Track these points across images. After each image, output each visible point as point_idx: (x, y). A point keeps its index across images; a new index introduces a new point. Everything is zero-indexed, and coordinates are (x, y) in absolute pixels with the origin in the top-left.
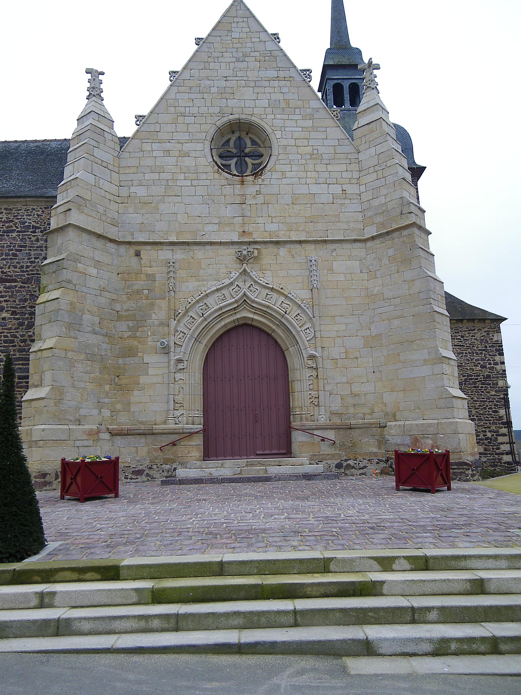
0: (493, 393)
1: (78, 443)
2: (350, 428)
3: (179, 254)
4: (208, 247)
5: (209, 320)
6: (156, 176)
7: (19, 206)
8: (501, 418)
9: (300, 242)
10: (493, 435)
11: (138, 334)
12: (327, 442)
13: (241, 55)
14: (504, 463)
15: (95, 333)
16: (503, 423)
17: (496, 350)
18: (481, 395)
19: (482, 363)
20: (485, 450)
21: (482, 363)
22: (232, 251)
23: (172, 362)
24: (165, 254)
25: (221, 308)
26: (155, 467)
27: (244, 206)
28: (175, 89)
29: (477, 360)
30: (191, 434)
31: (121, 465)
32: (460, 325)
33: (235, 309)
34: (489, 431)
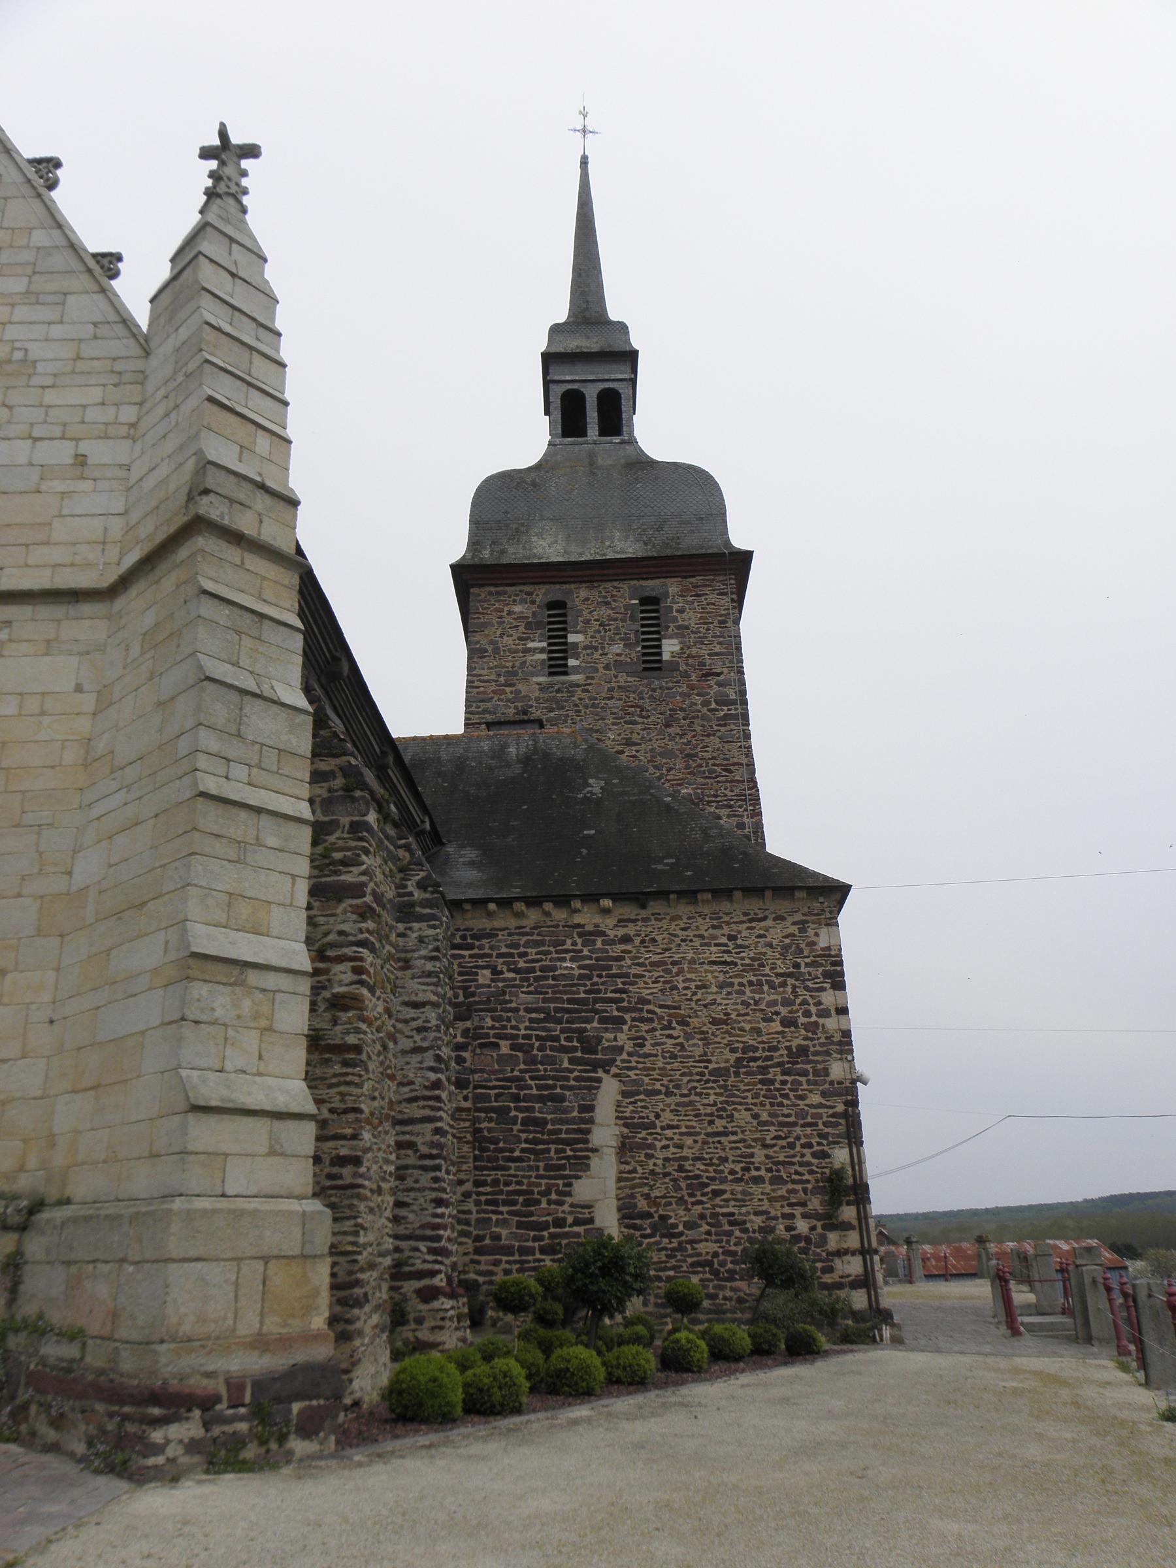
0: (816, 1099)
10: (813, 1228)
17: (826, 975)
19: (784, 1011)
21: (784, 1011)
32: (726, 906)
34: (805, 1216)
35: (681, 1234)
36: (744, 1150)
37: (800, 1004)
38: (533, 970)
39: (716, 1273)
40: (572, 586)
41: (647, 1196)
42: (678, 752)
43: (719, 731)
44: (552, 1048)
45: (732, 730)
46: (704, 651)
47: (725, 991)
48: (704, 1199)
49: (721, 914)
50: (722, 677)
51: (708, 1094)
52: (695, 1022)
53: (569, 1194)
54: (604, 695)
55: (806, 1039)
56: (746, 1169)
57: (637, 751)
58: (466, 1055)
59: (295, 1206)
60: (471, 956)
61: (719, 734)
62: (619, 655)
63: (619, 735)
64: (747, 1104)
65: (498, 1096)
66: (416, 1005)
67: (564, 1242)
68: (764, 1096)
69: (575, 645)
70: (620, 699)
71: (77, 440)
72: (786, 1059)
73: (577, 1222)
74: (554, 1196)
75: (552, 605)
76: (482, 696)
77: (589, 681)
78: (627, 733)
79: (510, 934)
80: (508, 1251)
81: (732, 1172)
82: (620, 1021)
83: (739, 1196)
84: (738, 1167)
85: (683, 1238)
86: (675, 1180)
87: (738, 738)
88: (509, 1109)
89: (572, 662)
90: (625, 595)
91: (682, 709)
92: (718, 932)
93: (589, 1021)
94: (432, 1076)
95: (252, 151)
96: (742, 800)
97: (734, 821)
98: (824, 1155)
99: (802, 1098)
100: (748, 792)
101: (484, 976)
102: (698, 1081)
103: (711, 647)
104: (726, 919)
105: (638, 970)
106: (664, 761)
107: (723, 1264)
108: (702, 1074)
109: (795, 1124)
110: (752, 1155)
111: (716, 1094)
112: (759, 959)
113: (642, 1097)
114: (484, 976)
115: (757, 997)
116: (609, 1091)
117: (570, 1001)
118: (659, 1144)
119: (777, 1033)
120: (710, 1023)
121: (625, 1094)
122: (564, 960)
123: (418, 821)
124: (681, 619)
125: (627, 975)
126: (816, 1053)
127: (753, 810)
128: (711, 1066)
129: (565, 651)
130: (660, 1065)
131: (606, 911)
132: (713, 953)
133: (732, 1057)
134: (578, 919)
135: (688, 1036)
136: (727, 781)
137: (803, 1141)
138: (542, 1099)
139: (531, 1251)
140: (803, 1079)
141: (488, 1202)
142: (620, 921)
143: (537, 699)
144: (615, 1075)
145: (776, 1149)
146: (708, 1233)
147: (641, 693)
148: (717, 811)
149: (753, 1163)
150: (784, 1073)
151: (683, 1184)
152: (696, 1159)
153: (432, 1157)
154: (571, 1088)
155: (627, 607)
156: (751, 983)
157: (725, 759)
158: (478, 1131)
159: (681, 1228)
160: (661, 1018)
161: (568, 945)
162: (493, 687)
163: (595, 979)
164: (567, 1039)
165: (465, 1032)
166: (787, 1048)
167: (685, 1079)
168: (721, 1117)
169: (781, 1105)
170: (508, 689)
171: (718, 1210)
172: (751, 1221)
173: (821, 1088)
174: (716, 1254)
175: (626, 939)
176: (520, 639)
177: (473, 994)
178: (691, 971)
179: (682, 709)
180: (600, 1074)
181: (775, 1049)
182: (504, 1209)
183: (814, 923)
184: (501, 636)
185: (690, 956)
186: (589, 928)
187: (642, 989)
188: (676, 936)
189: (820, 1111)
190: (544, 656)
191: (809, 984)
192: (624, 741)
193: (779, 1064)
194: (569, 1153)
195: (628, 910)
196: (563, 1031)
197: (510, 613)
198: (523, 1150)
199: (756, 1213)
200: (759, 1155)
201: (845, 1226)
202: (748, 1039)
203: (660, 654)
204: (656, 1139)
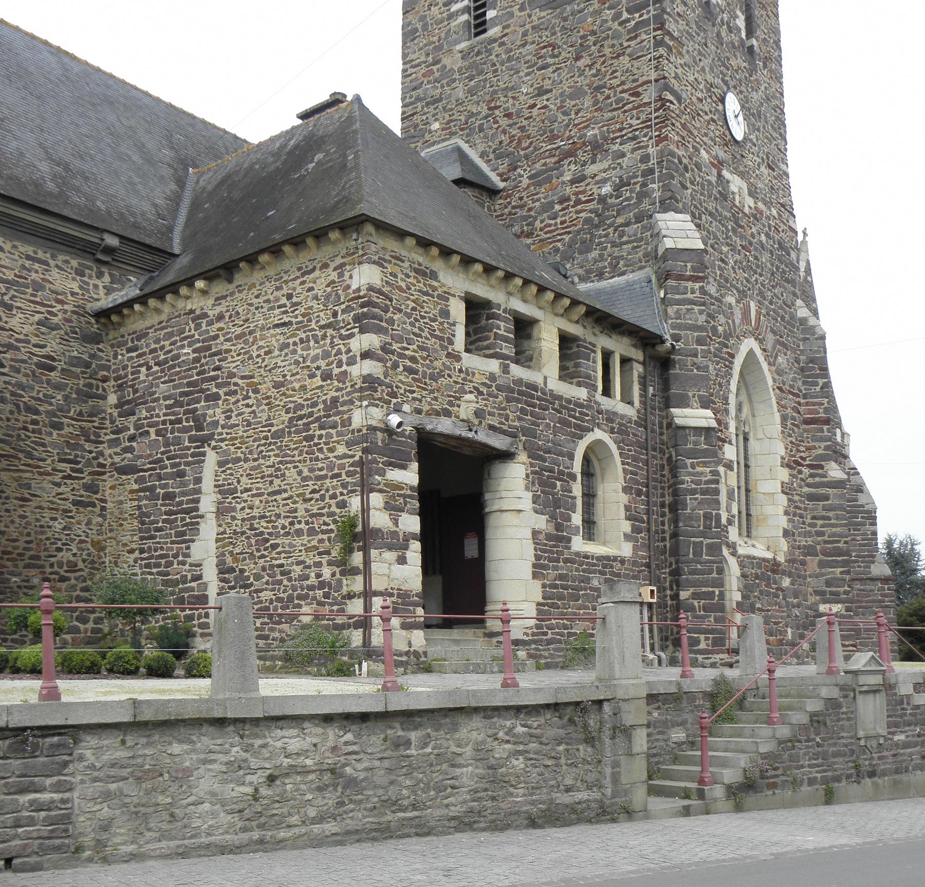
10: (333, 575)
21: (322, 363)
29: (315, 359)
35: (252, 584)
36: (292, 505)
37: (335, 355)
39: (270, 616)
42: (586, 88)
43: (629, 46)
45: (642, 41)
48: (266, 553)
49: (282, 274)
51: (269, 457)
54: (518, 43)
56: (292, 524)
57: (548, 100)
61: (628, 51)
63: (532, 86)
64: (294, 462)
67: (186, 595)
68: (307, 453)
70: (533, 42)
72: (322, 413)
74: (181, 558)
76: (414, 84)
77: (506, 31)
78: (539, 81)
81: (284, 527)
82: (216, 397)
83: (287, 549)
85: (252, 588)
86: (248, 538)
87: (648, 49)
91: (593, 33)
96: (648, 127)
99: (331, 450)
100: (654, 115)
102: (264, 445)
106: (573, 103)
108: (266, 438)
109: (325, 477)
110: (296, 511)
111: (275, 455)
113: (230, 465)
116: (211, 458)
118: (239, 507)
119: (318, 388)
120: (273, 387)
123: (97, 241)
127: (658, 136)
128: (273, 429)
130: (241, 434)
132: (276, 316)
136: (635, 108)
140: (333, 431)
142: (217, 299)
144: (214, 448)
145: (313, 502)
146: (267, 583)
147: (553, 27)
148: (621, 148)
149: (296, 517)
150: (321, 428)
156: (302, 341)
157: (634, 81)
159: (252, 579)
163: (203, 361)
166: (324, 402)
169: (317, 459)
172: (294, 571)
173: (346, 438)
174: (271, 601)
180: (207, 449)
181: (314, 405)
183: (350, 264)
187: (229, 365)
188: (251, 305)
189: (344, 461)
190: (465, 17)
191: (343, 332)
192: (536, 92)
193: (318, 419)
195: (220, 288)
198: (164, 521)
200: (301, 507)
201: (354, 571)
204: (237, 502)
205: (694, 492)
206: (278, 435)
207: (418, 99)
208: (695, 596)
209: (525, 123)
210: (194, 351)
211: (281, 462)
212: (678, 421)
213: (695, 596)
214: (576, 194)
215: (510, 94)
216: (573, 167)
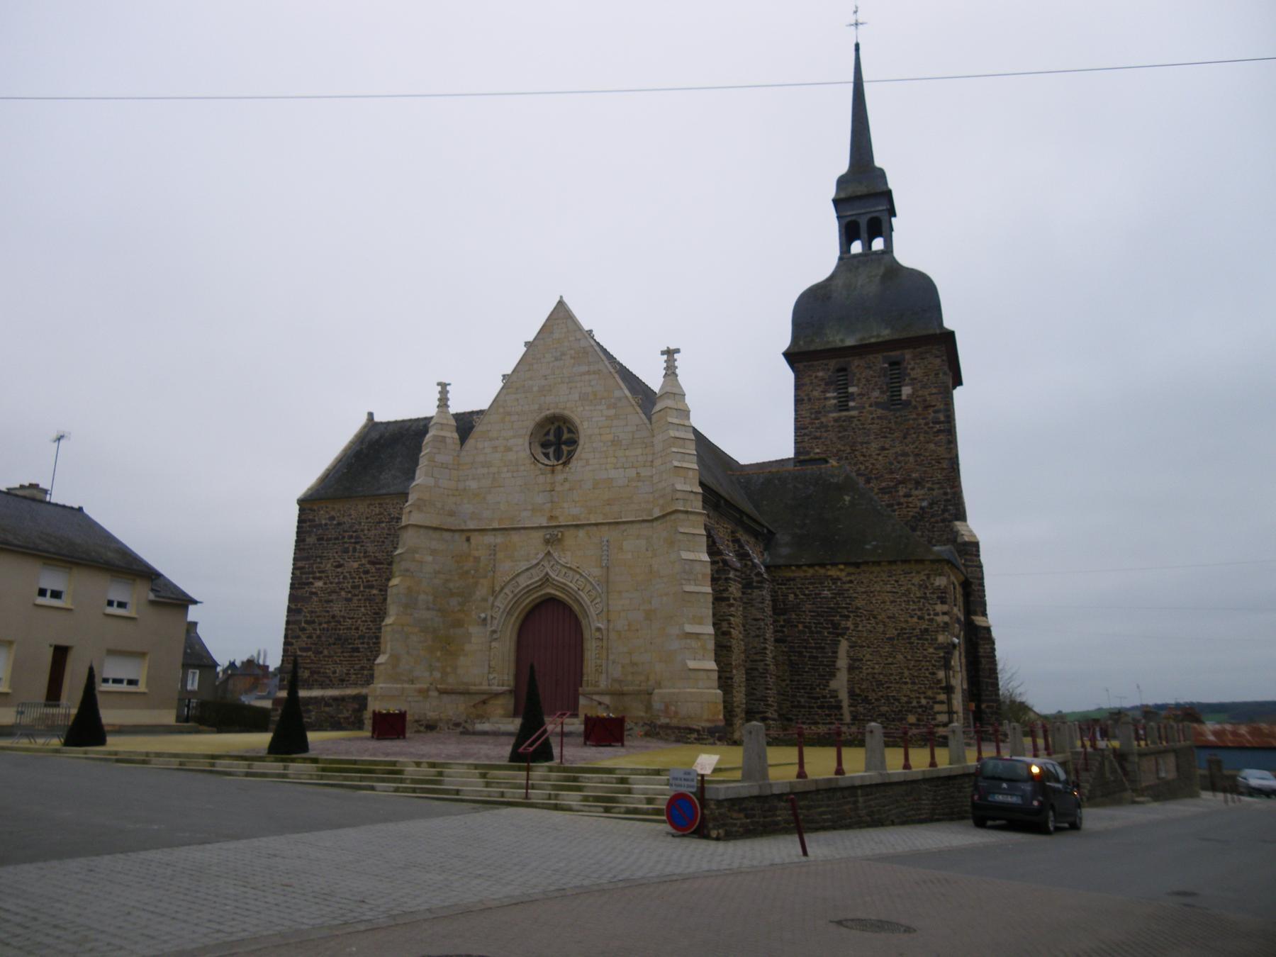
0: (931, 650)
1: (409, 699)
2: (622, 694)
3: (499, 539)
4: (522, 531)
5: (519, 596)
6: (485, 471)
7: (387, 501)
8: (939, 681)
9: (596, 525)
10: (928, 703)
11: (465, 609)
12: (603, 706)
13: (559, 354)
14: (939, 737)
15: (428, 609)
16: (942, 688)
17: (938, 598)
18: (916, 652)
19: (919, 613)
20: (918, 720)
21: (919, 613)
22: (540, 534)
23: (488, 633)
24: (489, 539)
25: (528, 586)
26: (469, 721)
27: (553, 492)
28: (505, 391)
29: (914, 610)
30: (497, 695)
31: (409, 718)
32: (894, 567)
33: (540, 586)
34: (925, 698)
35: (873, 703)
38: (811, 594)
39: (887, 718)
40: (850, 359)
41: (859, 688)
44: (820, 627)
46: (926, 392)
47: (893, 604)
50: (936, 408)
52: (880, 617)
53: (828, 686)
55: (928, 625)
58: (785, 629)
59: (713, 691)
60: (786, 588)
62: (877, 398)
65: (799, 647)
66: (756, 620)
69: (852, 394)
70: (878, 424)
71: (637, 468)
73: (831, 697)
75: (839, 370)
79: (802, 579)
80: (804, 707)
81: (895, 679)
84: (897, 678)
86: (871, 682)
88: (803, 652)
89: (852, 404)
90: (880, 362)
91: (913, 428)
92: (890, 579)
93: (835, 616)
94: (763, 645)
95: (677, 351)
97: (941, 491)
98: (934, 674)
99: (925, 650)
101: (791, 597)
103: (930, 390)
104: (894, 573)
105: (855, 595)
107: (890, 715)
108: (882, 639)
110: (903, 673)
112: (909, 590)
114: (791, 597)
115: (907, 607)
116: (844, 645)
117: (828, 608)
118: (864, 668)
121: (851, 647)
122: (824, 590)
124: (913, 374)
125: (850, 597)
126: (933, 631)
129: (847, 397)
131: (841, 570)
132: (888, 588)
133: (896, 632)
134: (829, 573)
135: (877, 624)
137: (925, 667)
138: (815, 648)
139: (813, 708)
140: (926, 642)
141: (795, 688)
143: (832, 426)
144: (847, 639)
146: (885, 703)
150: (918, 639)
151: (874, 684)
152: (880, 674)
153: (764, 673)
154: (828, 644)
155: (882, 369)
156: (905, 601)
157: (938, 456)
158: (791, 660)
160: (865, 616)
161: (826, 584)
162: (808, 420)
164: (827, 624)
165: (784, 620)
167: (876, 641)
168: (890, 657)
170: (817, 421)
171: (890, 694)
174: (887, 711)
175: (851, 582)
176: (822, 392)
177: (787, 605)
178: (879, 595)
179: (913, 428)
182: (802, 691)
184: (812, 391)
185: (878, 589)
186: (835, 577)
187: (859, 603)
190: (835, 401)
193: (917, 636)
194: (828, 670)
196: (825, 620)
197: (816, 377)
198: (809, 668)
199: (905, 696)
200: (906, 673)
202: (904, 625)
203: (900, 395)
205: (984, 657)
206: (891, 639)
207: (805, 435)
208: (988, 707)
209: (874, 462)
210: (831, 594)
211: (893, 651)
212: (977, 623)
213: (988, 707)
214: (907, 503)
215: (865, 445)
216: (904, 490)
